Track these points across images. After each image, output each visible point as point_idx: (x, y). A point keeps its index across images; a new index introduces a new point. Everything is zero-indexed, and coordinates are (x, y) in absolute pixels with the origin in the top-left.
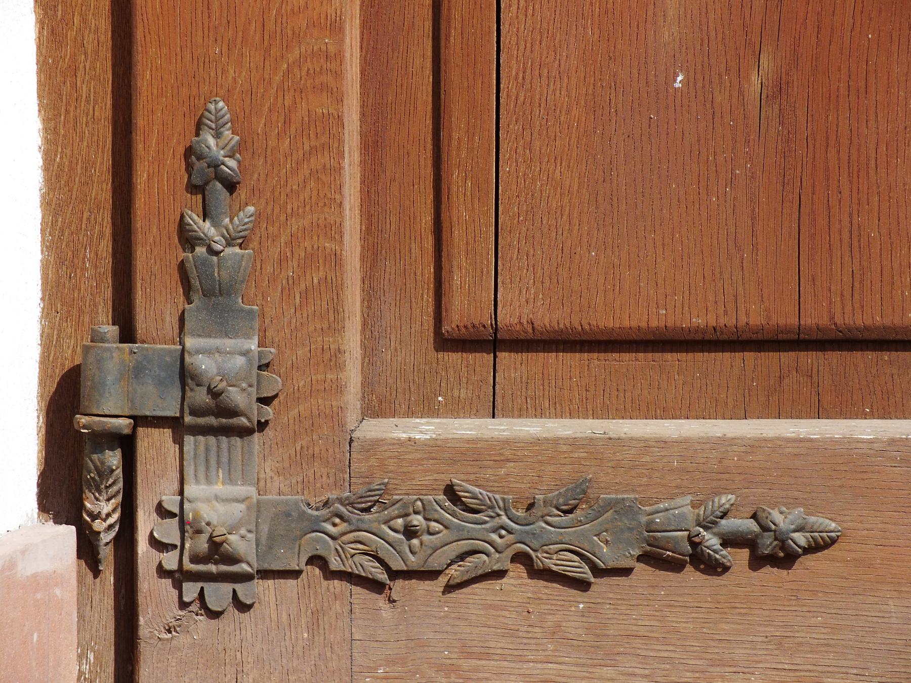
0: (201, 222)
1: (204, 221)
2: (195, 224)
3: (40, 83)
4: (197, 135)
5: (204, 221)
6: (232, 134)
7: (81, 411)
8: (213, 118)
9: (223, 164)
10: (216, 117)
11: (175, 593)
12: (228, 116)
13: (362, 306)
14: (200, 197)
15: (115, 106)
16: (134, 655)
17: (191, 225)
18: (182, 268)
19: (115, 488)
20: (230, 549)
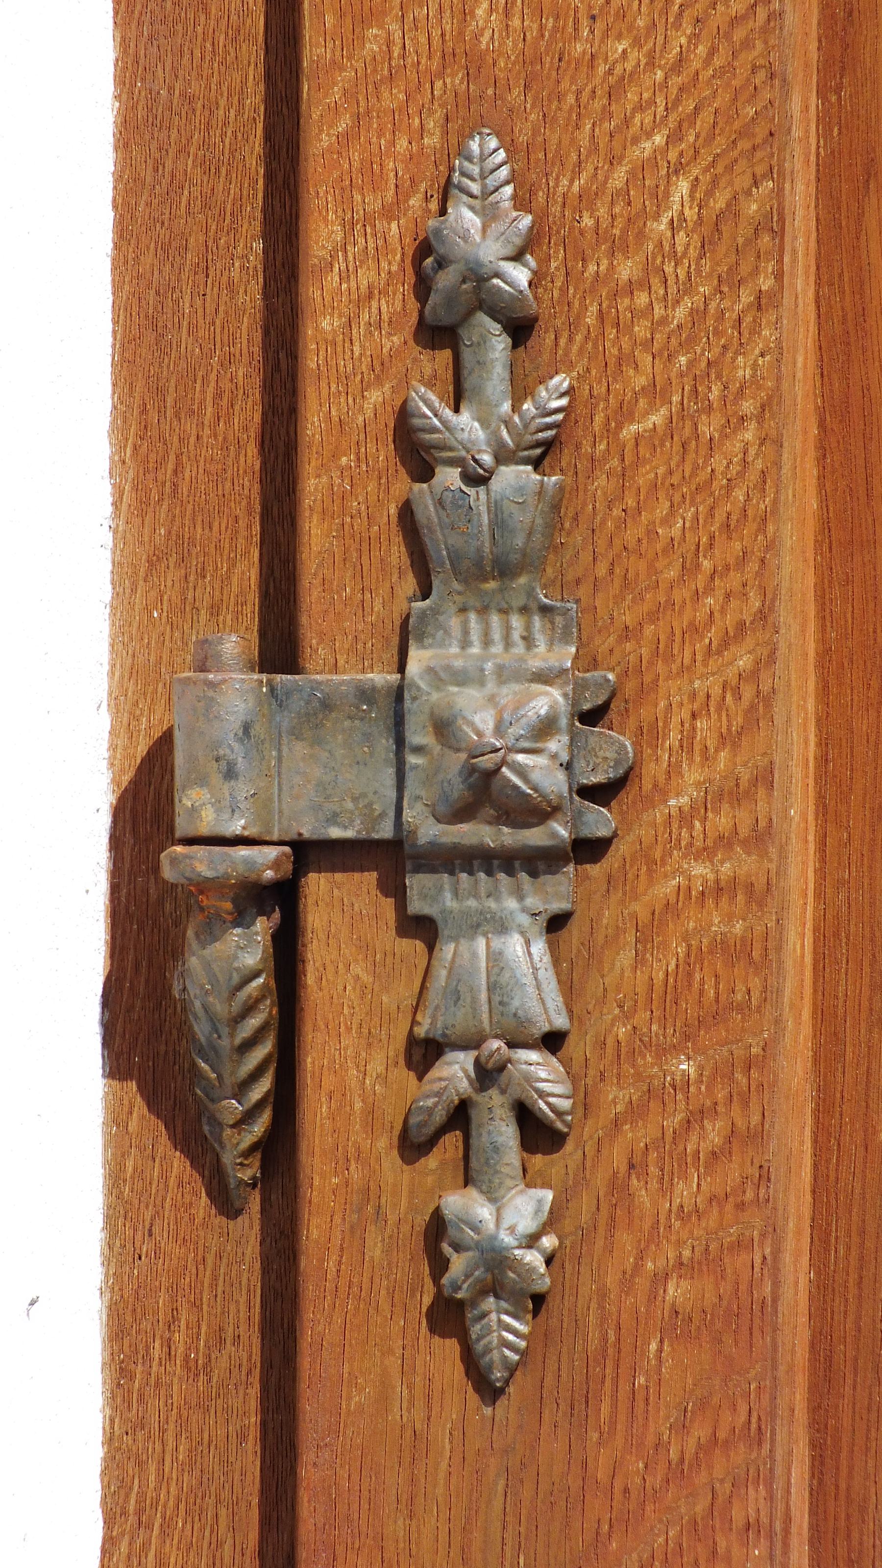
0: (448, 413)
1: (457, 410)
2: (436, 415)
3: (116, 307)
4: (443, 212)
5: (457, 410)
6: (516, 208)
7: (182, 826)
8: (475, 170)
9: (497, 275)
10: (484, 186)
11: (388, 905)
12: (504, 173)
13: (816, 819)
14: (447, 353)
15: (269, 77)
16: (297, 454)
17: (426, 417)
18: (407, 513)
19: (254, 1022)
20: (507, 288)
